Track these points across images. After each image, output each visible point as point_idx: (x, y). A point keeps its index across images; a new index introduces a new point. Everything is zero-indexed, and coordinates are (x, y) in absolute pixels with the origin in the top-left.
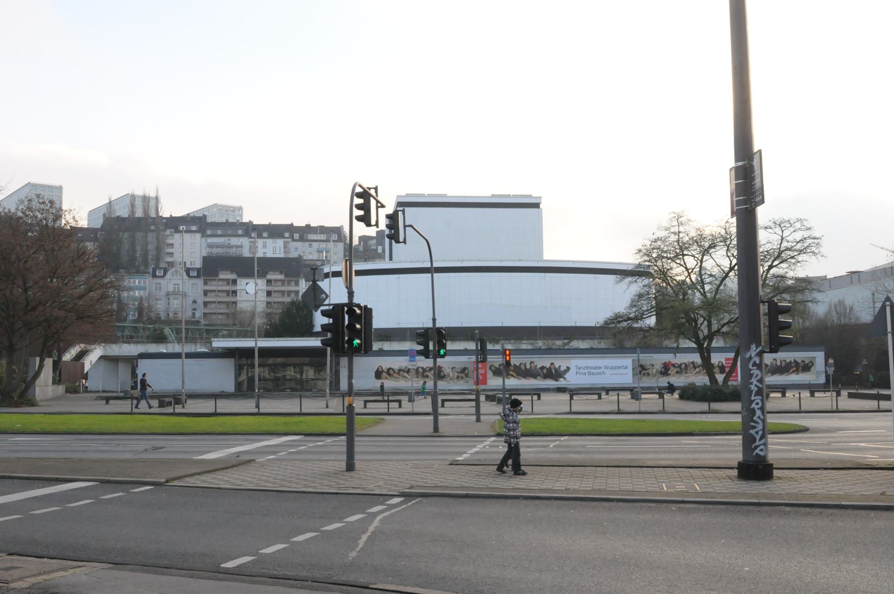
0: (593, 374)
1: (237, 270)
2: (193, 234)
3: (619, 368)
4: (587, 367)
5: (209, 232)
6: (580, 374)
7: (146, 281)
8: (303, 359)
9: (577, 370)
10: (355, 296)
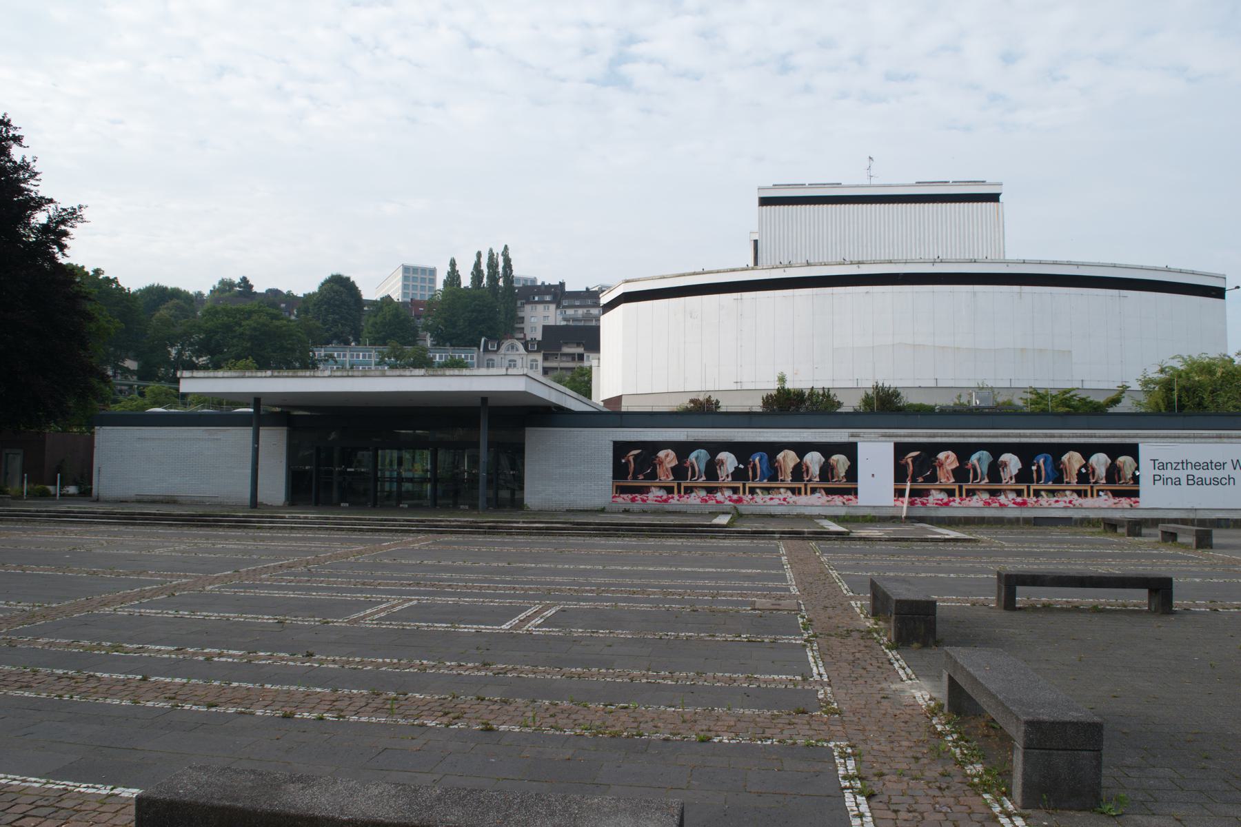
0: (1202, 482)
1: (584, 342)
2: (547, 305)
4: (1184, 464)
5: (565, 303)
6: (1165, 481)
7: (473, 356)
9: (1157, 472)
10: (173, 287)
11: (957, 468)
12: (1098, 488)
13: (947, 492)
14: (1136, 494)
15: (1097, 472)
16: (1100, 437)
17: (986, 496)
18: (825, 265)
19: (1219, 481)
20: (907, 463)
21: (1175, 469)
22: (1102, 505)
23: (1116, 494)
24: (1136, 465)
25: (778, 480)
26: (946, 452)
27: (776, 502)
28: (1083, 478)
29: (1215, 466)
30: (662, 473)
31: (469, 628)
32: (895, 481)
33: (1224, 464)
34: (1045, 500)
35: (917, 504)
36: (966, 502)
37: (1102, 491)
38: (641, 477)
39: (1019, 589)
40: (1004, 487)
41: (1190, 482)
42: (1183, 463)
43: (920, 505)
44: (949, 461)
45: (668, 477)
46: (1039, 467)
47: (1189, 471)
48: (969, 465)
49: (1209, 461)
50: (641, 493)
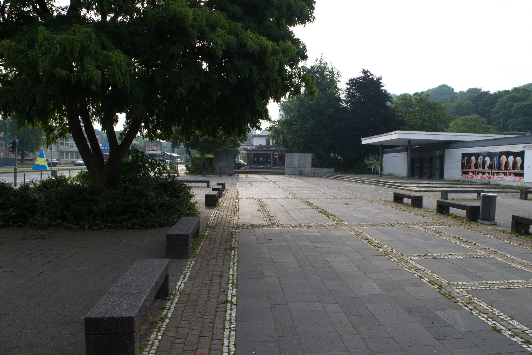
8: (452, 202)
23: (516, 175)
27: (500, 179)
39: (449, 194)
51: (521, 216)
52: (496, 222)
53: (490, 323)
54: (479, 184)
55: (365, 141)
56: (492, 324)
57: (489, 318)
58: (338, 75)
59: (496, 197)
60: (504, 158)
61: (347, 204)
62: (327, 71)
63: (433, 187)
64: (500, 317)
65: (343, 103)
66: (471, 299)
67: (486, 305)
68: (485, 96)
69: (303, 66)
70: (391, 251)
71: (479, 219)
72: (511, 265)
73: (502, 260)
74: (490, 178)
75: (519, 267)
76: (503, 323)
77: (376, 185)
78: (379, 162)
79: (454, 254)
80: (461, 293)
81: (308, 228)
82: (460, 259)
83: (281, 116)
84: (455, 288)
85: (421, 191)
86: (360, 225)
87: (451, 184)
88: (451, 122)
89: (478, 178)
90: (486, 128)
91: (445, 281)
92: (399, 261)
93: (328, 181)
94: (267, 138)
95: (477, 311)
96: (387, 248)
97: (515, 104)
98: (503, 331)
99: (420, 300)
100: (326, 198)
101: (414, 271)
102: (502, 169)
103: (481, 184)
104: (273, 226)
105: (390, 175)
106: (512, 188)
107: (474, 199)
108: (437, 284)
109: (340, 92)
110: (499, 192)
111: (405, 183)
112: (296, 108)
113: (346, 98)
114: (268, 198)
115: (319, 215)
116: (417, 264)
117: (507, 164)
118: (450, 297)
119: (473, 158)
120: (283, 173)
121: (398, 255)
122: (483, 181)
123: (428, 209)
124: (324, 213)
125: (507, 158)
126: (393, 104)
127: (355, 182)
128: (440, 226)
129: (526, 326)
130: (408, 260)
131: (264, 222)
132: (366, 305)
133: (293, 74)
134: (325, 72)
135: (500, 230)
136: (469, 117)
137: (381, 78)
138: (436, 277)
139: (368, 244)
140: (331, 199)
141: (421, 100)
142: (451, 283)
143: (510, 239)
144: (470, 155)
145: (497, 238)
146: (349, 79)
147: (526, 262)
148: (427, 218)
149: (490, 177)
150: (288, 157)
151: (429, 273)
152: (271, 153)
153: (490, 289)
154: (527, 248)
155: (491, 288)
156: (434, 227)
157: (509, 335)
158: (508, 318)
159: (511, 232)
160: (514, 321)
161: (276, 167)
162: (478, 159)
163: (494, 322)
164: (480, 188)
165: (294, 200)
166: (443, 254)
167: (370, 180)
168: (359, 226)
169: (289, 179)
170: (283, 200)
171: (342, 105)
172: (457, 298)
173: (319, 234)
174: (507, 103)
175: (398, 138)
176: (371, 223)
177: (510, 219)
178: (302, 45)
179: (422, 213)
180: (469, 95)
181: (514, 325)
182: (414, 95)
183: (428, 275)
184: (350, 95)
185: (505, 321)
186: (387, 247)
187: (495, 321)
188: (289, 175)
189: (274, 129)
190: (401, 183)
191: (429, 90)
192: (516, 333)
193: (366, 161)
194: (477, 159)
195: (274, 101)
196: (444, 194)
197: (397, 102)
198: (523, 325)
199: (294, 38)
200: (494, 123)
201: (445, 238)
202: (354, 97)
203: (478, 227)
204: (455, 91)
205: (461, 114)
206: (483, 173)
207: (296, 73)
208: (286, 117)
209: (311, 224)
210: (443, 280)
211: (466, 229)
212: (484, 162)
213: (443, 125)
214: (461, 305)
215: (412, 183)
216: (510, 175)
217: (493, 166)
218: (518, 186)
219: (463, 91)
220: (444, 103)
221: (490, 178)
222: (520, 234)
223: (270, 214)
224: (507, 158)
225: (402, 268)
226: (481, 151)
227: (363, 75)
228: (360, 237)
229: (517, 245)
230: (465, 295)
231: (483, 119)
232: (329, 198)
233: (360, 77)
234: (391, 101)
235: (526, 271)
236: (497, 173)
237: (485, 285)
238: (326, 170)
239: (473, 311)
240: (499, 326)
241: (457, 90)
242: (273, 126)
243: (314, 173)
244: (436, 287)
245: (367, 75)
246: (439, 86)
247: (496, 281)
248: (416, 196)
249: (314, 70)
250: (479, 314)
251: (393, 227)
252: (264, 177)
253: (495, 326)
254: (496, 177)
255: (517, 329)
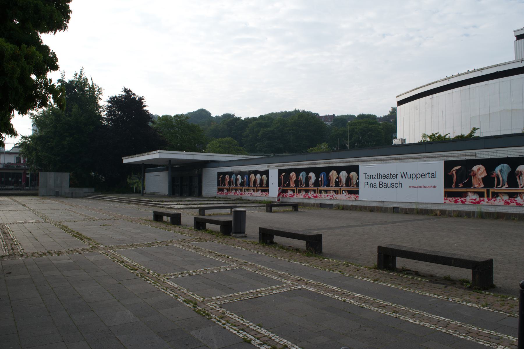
0: (386, 186)
3: (423, 176)
8: (208, 218)
11: (485, 177)
12: (342, 189)
13: (507, 194)
14: (356, 192)
15: (342, 181)
16: (344, 162)
17: (506, 198)
18: (466, 74)
19: (394, 185)
20: (453, 174)
21: (374, 179)
22: (343, 198)
23: (350, 192)
24: (358, 177)
25: (329, 187)
26: (478, 166)
27: (250, 195)
28: (337, 184)
29: (393, 176)
30: (291, 183)
31: (430, 320)
32: (445, 187)
33: (397, 175)
34: (324, 195)
35: (459, 202)
36: (492, 201)
37: (344, 190)
38: (461, 185)
39: (206, 210)
40: (310, 189)
41: (381, 186)
42: (377, 175)
43: (460, 203)
44: (480, 172)
45: (480, 185)
46: (321, 179)
47: (381, 180)
48: (494, 175)
49: (389, 174)
50: (461, 197)
51: (266, 228)
52: (246, 235)
53: (241, 336)
54: (233, 200)
55: (126, 160)
56: (243, 335)
57: (240, 330)
58: (99, 92)
59: (246, 211)
60: (252, 176)
61: (105, 225)
62: (87, 87)
63: (192, 204)
64: (249, 327)
65: (104, 121)
66: (223, 313)
67: (237, 317)
68: (237, 121)
69: (61, 80)
70: (148, 272)
71: (231, 233)
72: (259, 274)
73: (251, 270)
74: (241, 194)
75: (266, 275)
76: (253, 333)
77: (137, 204)
78: (141, 181)
79: (209, 269)
80: (214, 308)
81: (58, 255)
82: (214, 273)
83: (35, 131)
84: (209, 304)
85: (180, 209)
86: (117, 247)
87: (208, 201)
88: (208, 143)
89: (232, 194)
90: (238, 150)
91: (200, 298)
92: (155, 282)
93: (87, 201)
94: (17, 155)
95: (230, 325)
96: (144, 270)
97: (261, 129)
98: (253, 342)
99: (175, 322)
100: (83, 220)
101: (169, 291)
102: (251, 186)
103: (235, 200)
104: (15, 256)
105: (152, 194)
106: (260, 202)
107: (228, 214)
108: (192, 302)
109: (101, 109)
110: (249, 206)
111: (166, 201)
112: (52, 123)
113: (107, 116)
114: (13, 223)
115: (72, 239)
116: (173, 283)
117: (255, 181)
118: (204, 314)
119: (227, 176)
120: (36, 195)
121: (155, 276)
122: (236, 197)
123: (186, 226)
124: (78, 237)
125: (255, 176)
126: (154, 124)
127: (116, 201)
128: (197, 241)
129: (272, 333)
130: (165, 280)
131: (5, 252)
132: (118, 337)
133: (39, 84)
134: (85, 88)
135: (250, 242)
136: (224, 139)
137: (143, 98)
138: (192, 294)
139: (124, 267)
140: (88, 221)
141: (181, 122)
142: (206, 299)
143: (258, 250)
144: (225, 174)
145: (247, 249)
146: (111, 96)
147: (272, 270)
148: (185, 235)
149: (242, 193)
150: (42, 176)
151: (184, 291)
152: (22, 172)
153: (241, 300)
154: (272, 257)
155: (242, 299)
156: (191, 244)
157: (258, 344)
158: (257, 327)
159: (258, 243)
160: (262, 329)
161: (28, 188)
162: (231, 178)
163: (245, 333)
164: (234, 203)
165: (46, 223)
166: (199, 270)
167: (132, 199)
168: (116, 248)
169: (42, 201)
170: (32, 225)
171: (103, 123)
172: (211, 314)
173: (71, 261)
174: (255, 128)
175: (159, 157)
176: (129, 244)
177: (258, 231)
178: (51, 54)
179: (180, 230)
180: (223, 120)
181: (262, 334)
182: (174, 116)
183: (183, 293)
184: (111, 113)
185: (254, 330)
186: (144, 269)
187: (245, 332)
188: (43, 196)
189: (26, 146)
190: (162, 201)
191: (189, 113)
192: (264, 341)
193: (128, 180)
194: (230, 178)
195: (19, 113)
196: (202, 211)
197: (158, 122)
198: (270, 332)
199: (42, 44)
200: (244, 146)
201: (201, 253)
202: (115, 115)
203: (231, 240)
204: (212, 116)
205: (217, 137)
206: (236, 190)
207: (42, 82)
208: (40, 132)
209: (62, 250)
210: (198, 298)
211: (220, 243)
212: (237, 180)
213: (202, 146)
214: (215, 320)
215: (172, 201)
216: (258, 191)
217: (244, 183)
218: (264, 201)
219: (219, 116)
220: (202, 126)
221: (241, 194)
222: (267, 244)
223: (13, 242)
224: (255, 176)
225: (158, 290)
226: (234, 170)
227: (124, 94)
228: (116, 260)
229: (264, 254)
230: (218, 309)
231: (235, 142)
232: (86, 220)
233: (121, 96)
234: (153, 122)
235: (271, 278)
236: (326, 191)
237: (236, 297)
238: (86, 190)
239: (225, 326)
240: (250, 337)
241: (214, 115)
242: (24, 142)
243: (72, 193)
244: (191, 305)
245: (129, 94)
246: (198, 110)
247: (246, 291)
248: (174, 214)
249: (73, 85)
250: (231, 328)
251: (152, 247)
252: (13, 199)
253: (246, 337)
254: (246, 193)
255: (265, 337)
